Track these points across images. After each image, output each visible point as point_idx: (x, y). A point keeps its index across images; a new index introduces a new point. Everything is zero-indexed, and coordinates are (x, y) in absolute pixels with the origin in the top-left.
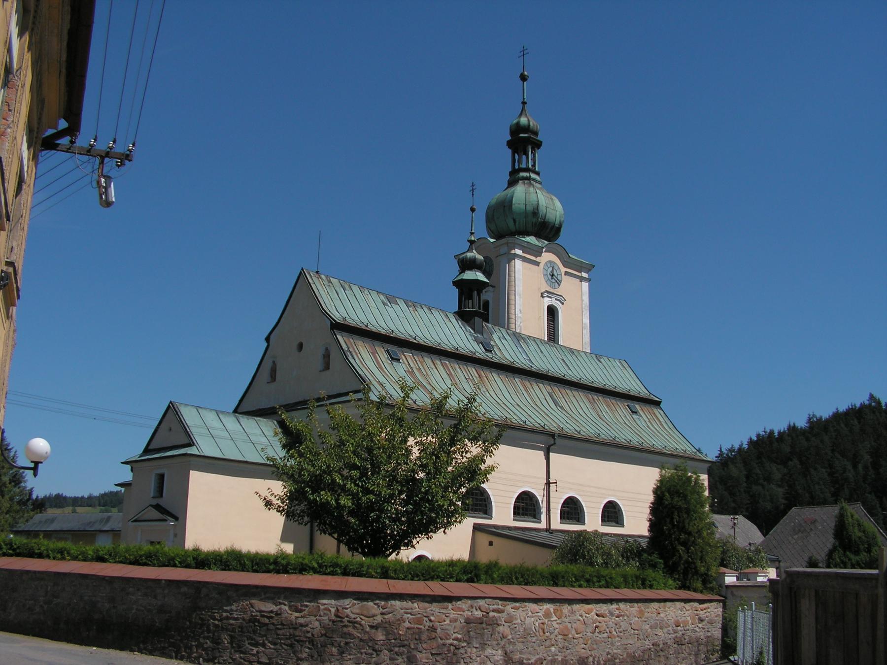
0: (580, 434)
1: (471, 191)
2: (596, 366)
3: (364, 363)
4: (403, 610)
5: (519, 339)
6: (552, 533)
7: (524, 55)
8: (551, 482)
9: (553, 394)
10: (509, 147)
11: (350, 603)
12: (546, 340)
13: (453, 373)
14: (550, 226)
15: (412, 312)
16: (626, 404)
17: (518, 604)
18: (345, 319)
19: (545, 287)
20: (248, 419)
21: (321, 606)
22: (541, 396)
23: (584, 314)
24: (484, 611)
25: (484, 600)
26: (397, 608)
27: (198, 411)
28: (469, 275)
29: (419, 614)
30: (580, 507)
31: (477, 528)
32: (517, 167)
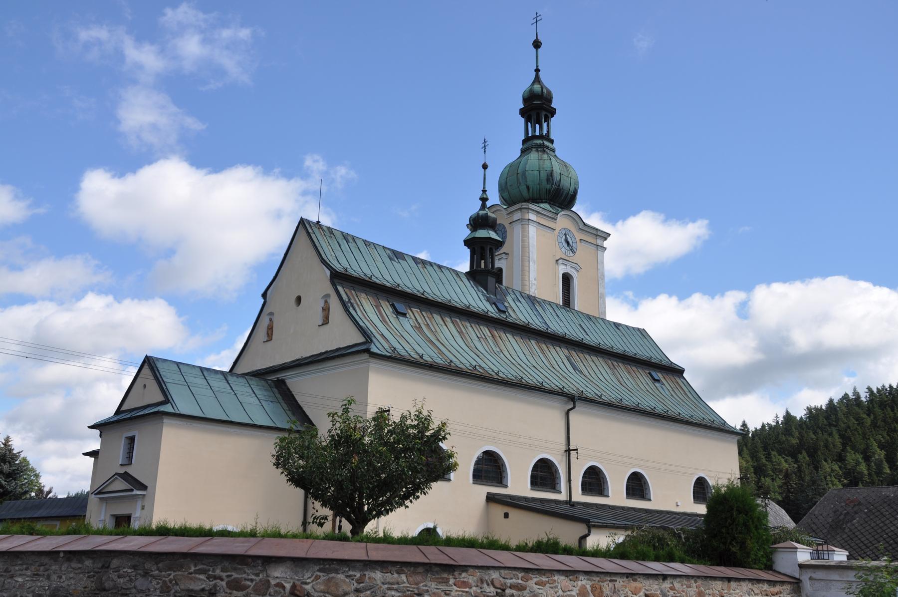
0: (601, 398)
1: (482, 148)
2: (614, 333)
3: (366, 315)
4: (386, 586)
5: (535, 302)
6: (573, 505)
7: (537, 22)
8: (571, 449)
9: (572, 358)
10: (523, 116)
11: (312, 575)
12: (562, 304)
13: (464, 332)
14: (564, 194)
15: (421, 269)
16: (648, 372)
17: (544, 579)
18: (346, 270)
19: (560, 253)
20: (237, 378)
21: (271, 581)
22: (558, 359)
23: (601, 284)
24: (499, 586)
25: (498, 571)
26: (379, 582)
27: (179, 368)
28: (482, 233)
29: (408, 591)
30: (603, 478)
31: (491, 499)
32: (530, 135)
